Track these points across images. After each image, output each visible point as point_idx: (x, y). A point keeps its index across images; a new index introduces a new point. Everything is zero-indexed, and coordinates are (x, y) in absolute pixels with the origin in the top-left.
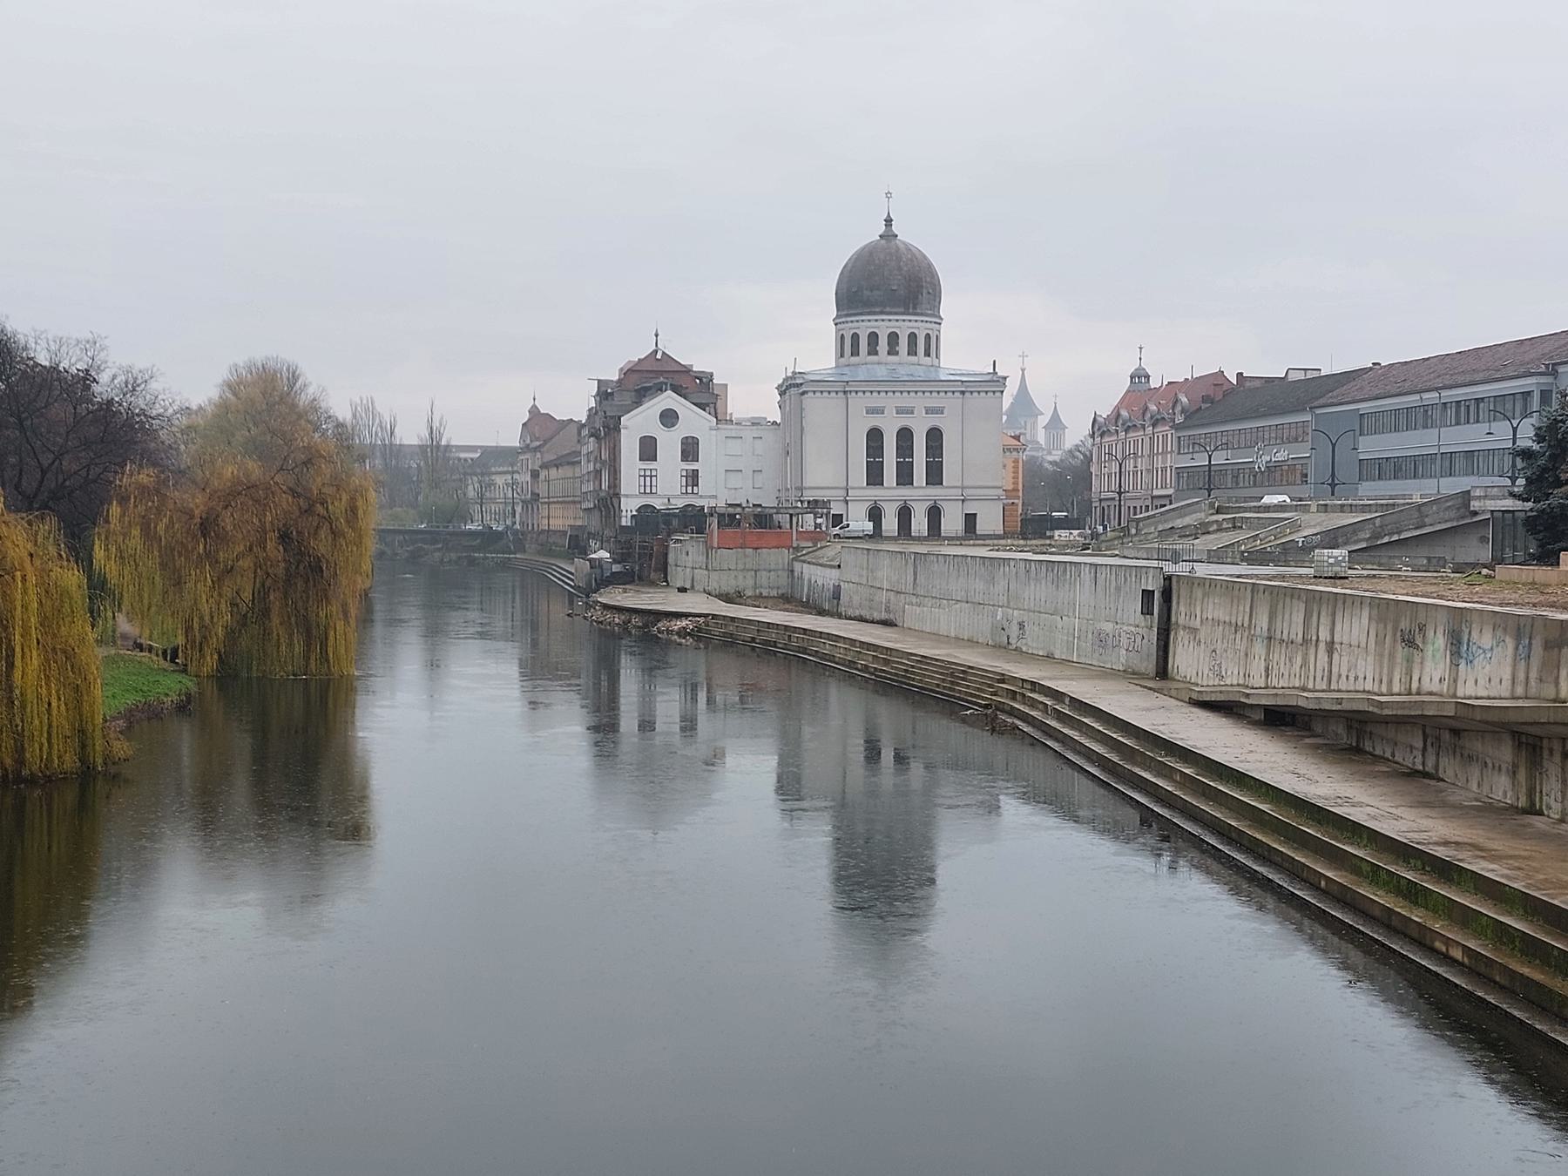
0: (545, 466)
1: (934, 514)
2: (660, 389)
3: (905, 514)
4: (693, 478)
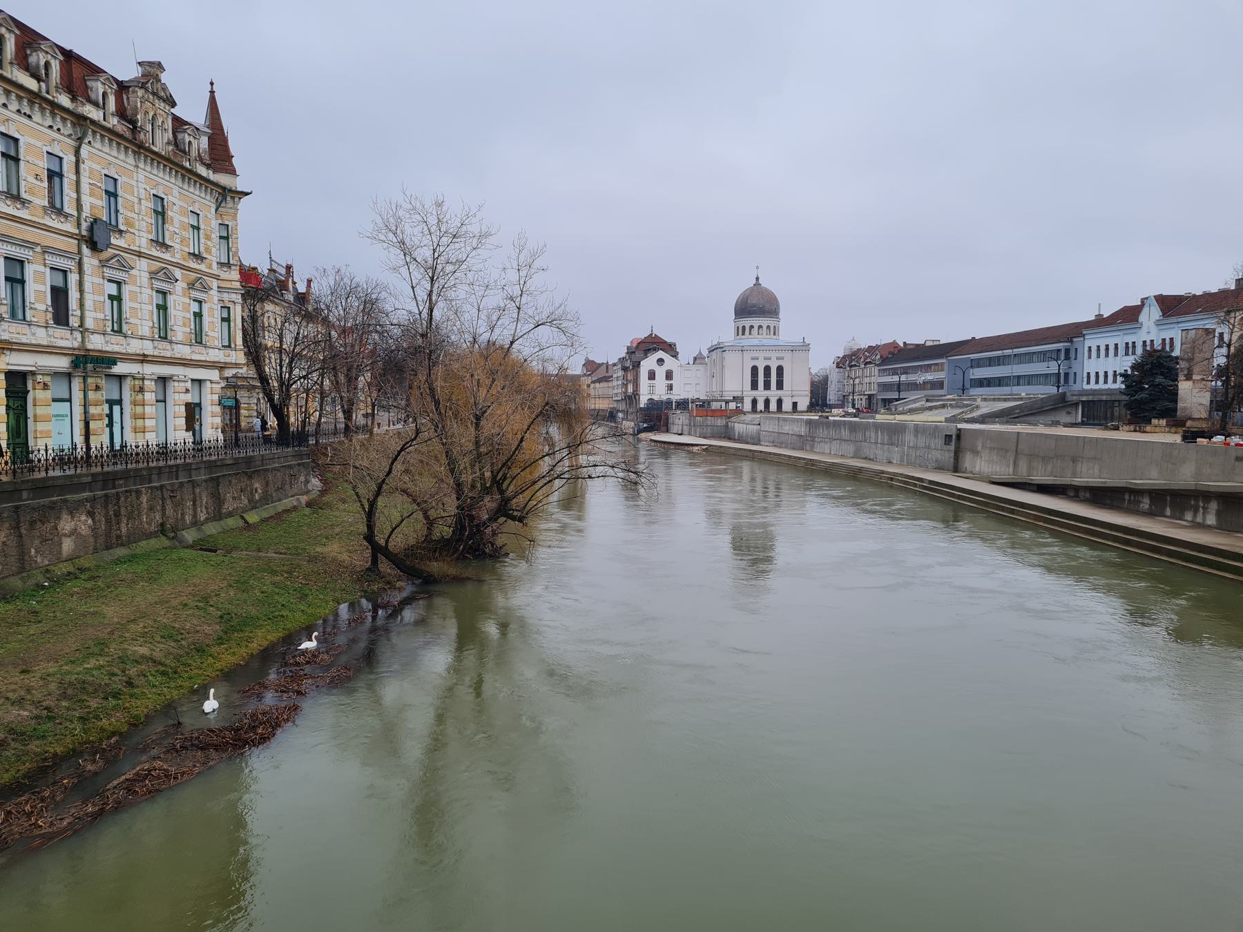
0: (593, 382)
1: (780, 402)
2: (655, 350)
3: (767, 402)
4: (670, 388)
